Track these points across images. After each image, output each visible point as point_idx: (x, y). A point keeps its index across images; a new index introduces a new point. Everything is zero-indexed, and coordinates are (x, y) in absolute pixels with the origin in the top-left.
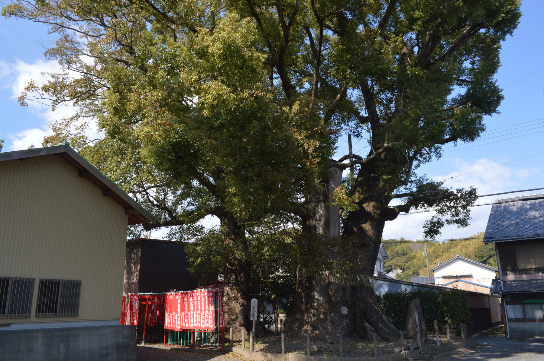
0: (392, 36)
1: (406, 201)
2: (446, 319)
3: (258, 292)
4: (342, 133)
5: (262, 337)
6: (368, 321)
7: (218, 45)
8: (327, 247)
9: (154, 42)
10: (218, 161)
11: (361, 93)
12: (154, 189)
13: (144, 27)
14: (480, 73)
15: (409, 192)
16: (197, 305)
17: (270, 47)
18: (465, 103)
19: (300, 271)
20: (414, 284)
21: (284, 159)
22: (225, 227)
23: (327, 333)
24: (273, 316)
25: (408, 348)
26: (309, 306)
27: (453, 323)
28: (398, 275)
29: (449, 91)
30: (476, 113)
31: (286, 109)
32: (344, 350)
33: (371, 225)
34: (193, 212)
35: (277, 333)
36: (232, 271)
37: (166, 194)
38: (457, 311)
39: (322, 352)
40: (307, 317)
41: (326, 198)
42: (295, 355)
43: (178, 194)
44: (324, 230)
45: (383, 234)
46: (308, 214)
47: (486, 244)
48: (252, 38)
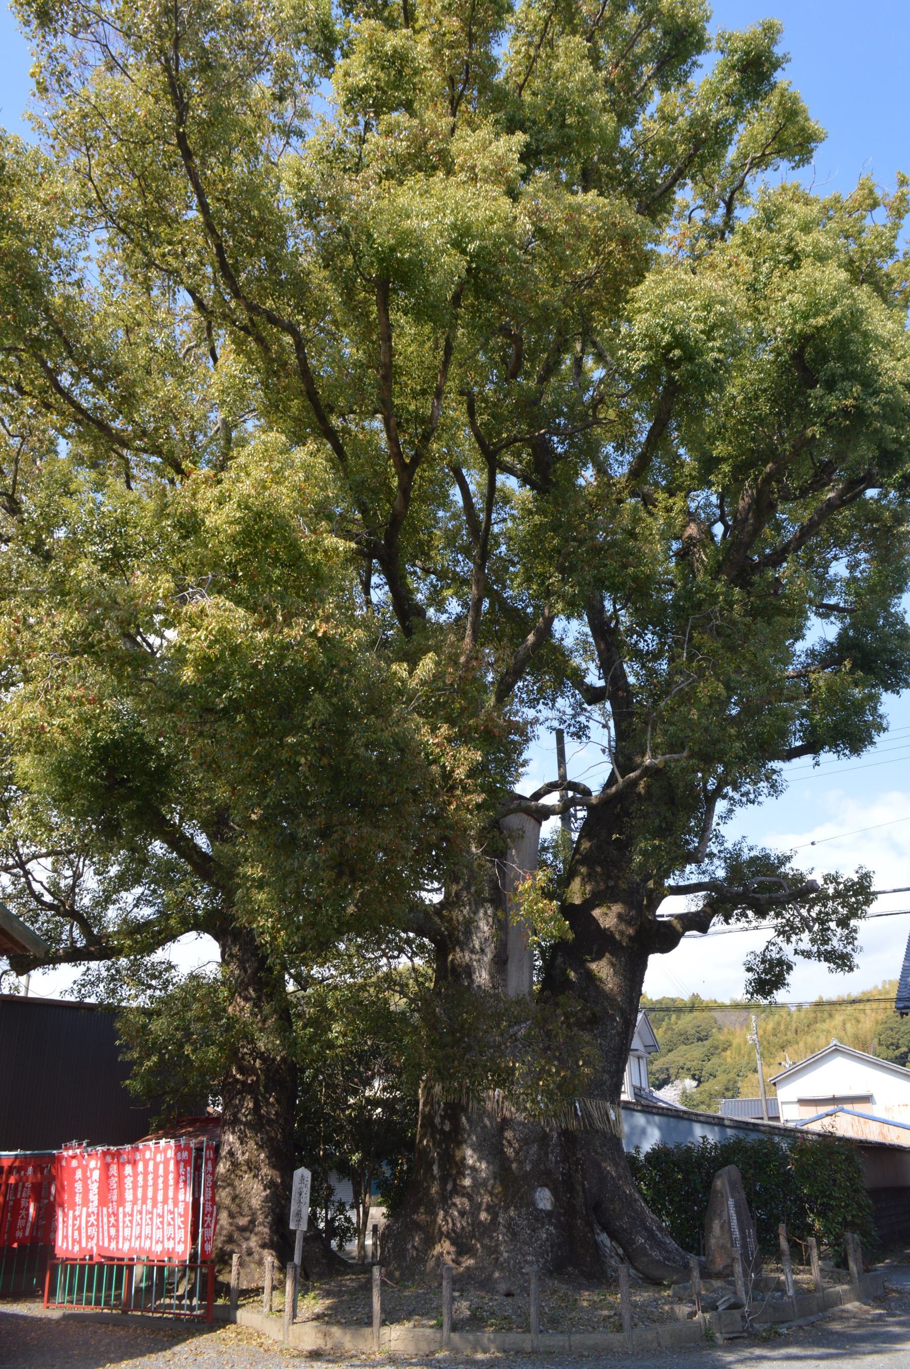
0: (661, 496)
1: (701, 904)
2: (809, 1220)
3: (316, 1145)
4: (540, 730)
5: (320, 1277)
6: (605, 1228)
7: (230, 510)
8: (498, 1026)
9: (73, 487)
10: (222, 794)
11: (587, 630)
12: (48, 862)
13: (52, 450)
14: (872, 590)
15: (707, 880)
16: (145, 1187)
17: (364, 511)
18: (839, 662)
19: (428, 1089)
20: (727, 1123)
21: (393, 792)
22: (233, 966)
23: (497, 1264)
24: (352, 1215)
25: (711, 1307)
26: (449, 1187)
27: (828, 1231)
28: (686, 1097)
29: (799, 635)
30: (864, 687)
31: (401, 669)
32: (541, 1314)
33: (613, 965)
34: (148, 923)
35: (363, 1266)
36: (248, 1089)
37: (77, 876)
38: (836, 1199)
39: (482, 1319)
40: (445, 1219)
41: (499, 898)
42: (409, 1330)
43: (112, 874)
44: (492, 977)
45: (645, 989)
46: (451, 935)
47: (902, 1014)
48: (317, 494)
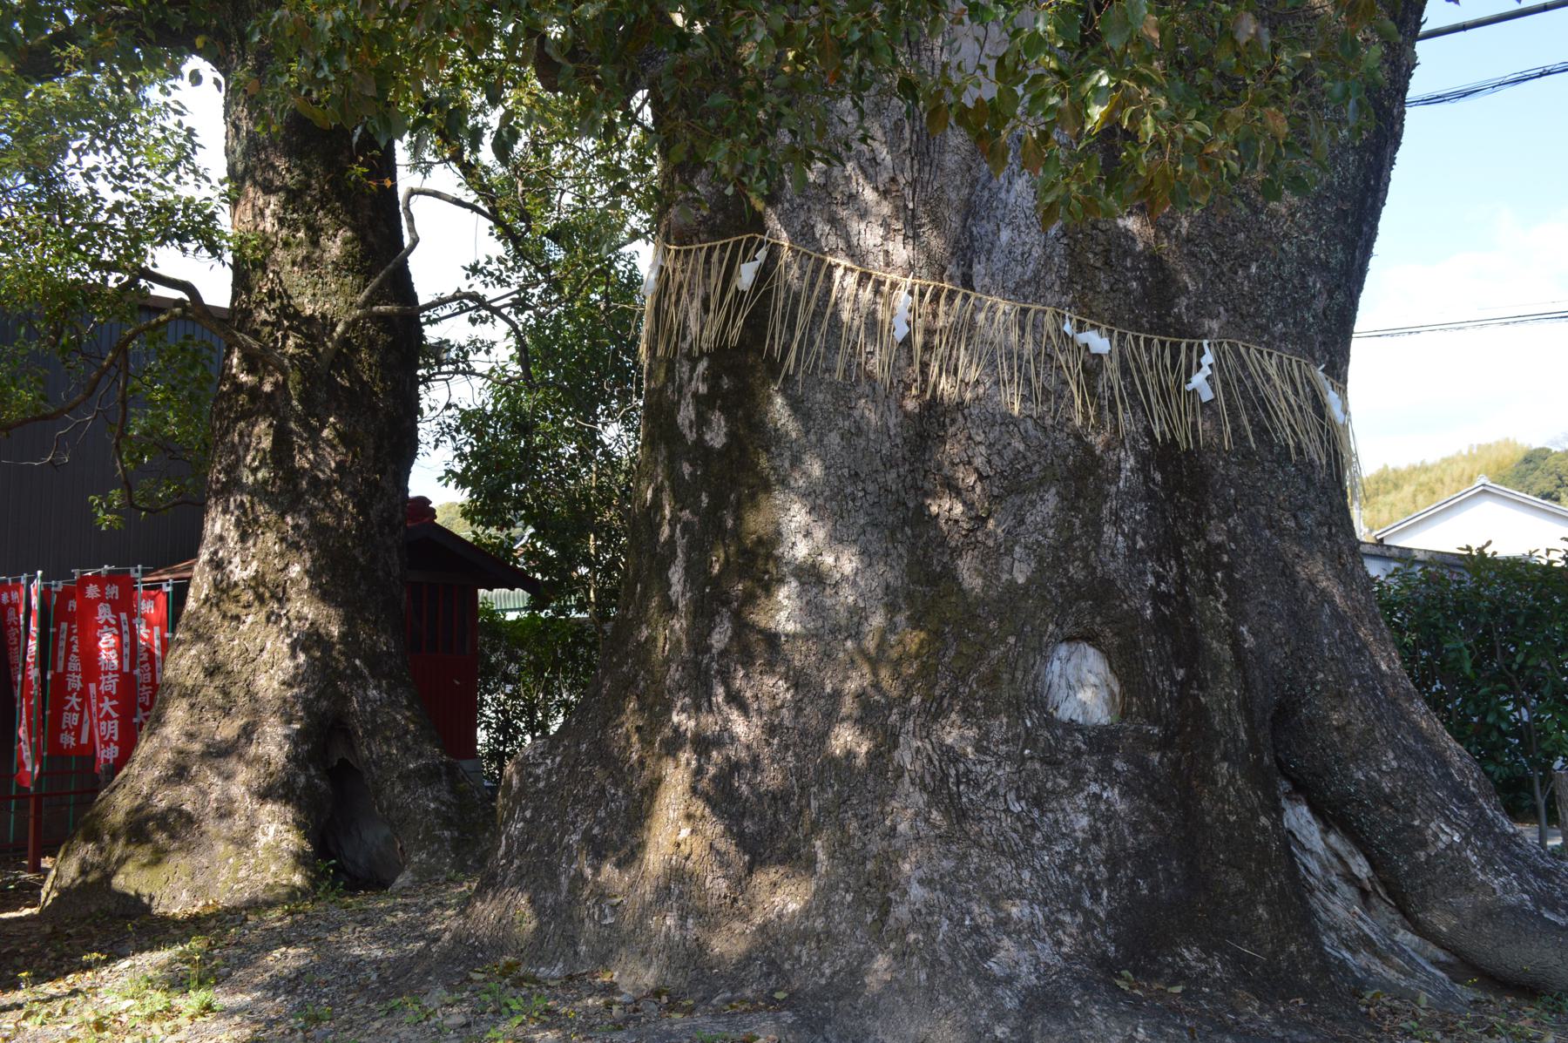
26: (719, 639)
